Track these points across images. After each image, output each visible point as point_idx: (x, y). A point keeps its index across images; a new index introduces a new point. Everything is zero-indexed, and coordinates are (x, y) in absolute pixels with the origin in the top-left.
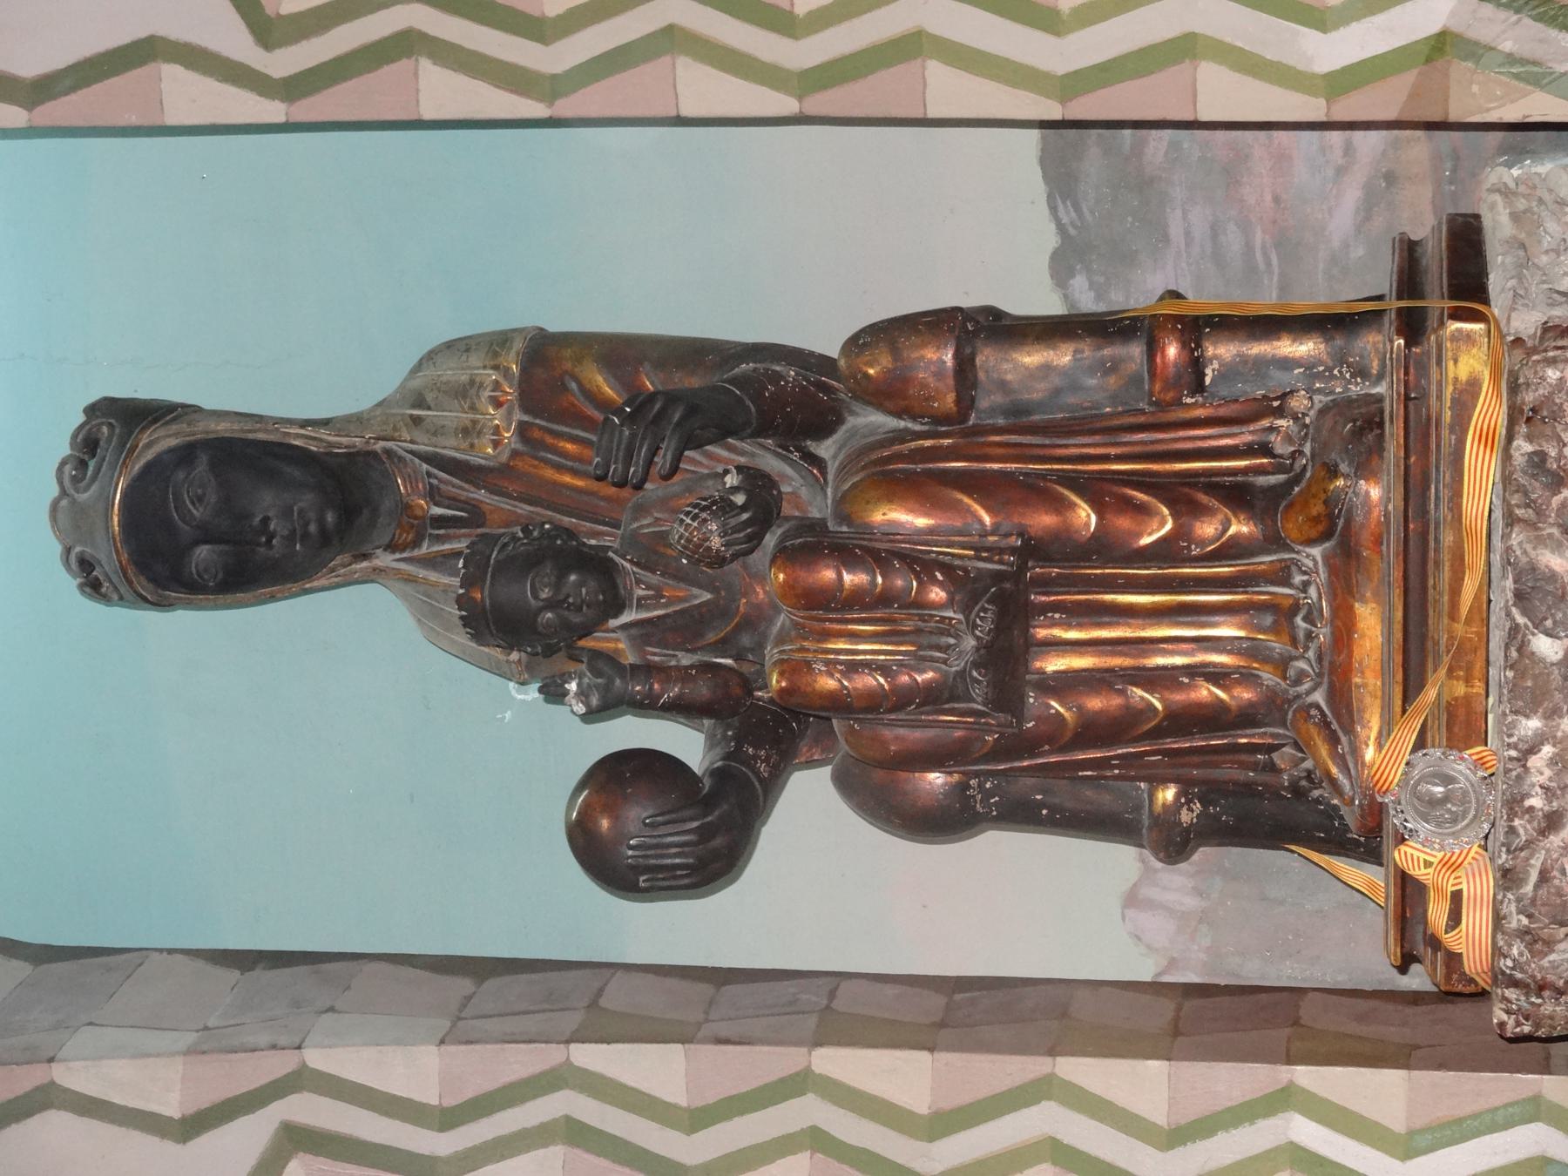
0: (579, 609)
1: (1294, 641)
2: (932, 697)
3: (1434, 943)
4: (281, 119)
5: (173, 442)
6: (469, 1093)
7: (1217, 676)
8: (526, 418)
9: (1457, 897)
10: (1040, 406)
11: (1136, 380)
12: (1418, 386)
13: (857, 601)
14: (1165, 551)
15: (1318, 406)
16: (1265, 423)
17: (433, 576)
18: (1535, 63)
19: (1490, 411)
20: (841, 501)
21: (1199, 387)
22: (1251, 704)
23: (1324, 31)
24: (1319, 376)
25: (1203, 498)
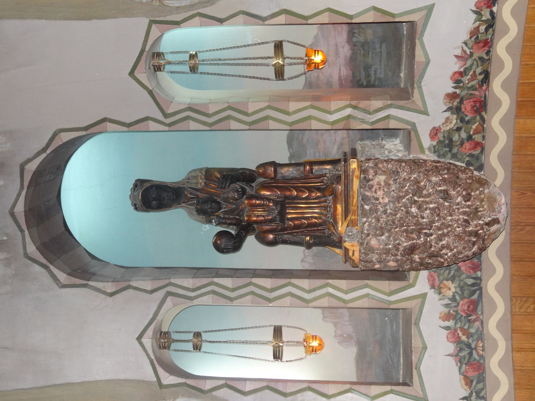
0: (214, 209)
1: (328, 212)
2: (271, 221)
3: (350, 258)
4: (168, 130)
5: (149, 185)
6: (197, 286)
7: (315, 218)
8: (206, 181)
9: (354, 251)
10: (287, 176)
11: (302, 172)
12: (346, 169)
13: (259, 205)
14: (307, 198)
15: (331, 175)
16: (323, 178)
17: (191, 207)
18: (364, 119)
19: (357, 173)
20: (256, 190)
21: (312, 173)
22: (321, 222)
23: (331, 115)
24: (331, 171)
25: (313, 189)
